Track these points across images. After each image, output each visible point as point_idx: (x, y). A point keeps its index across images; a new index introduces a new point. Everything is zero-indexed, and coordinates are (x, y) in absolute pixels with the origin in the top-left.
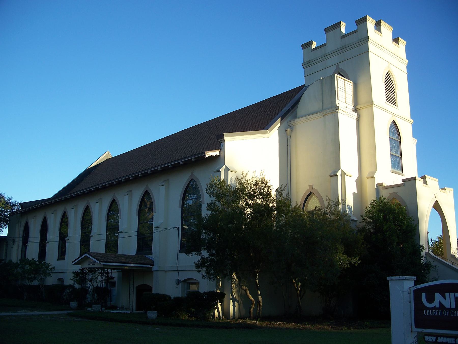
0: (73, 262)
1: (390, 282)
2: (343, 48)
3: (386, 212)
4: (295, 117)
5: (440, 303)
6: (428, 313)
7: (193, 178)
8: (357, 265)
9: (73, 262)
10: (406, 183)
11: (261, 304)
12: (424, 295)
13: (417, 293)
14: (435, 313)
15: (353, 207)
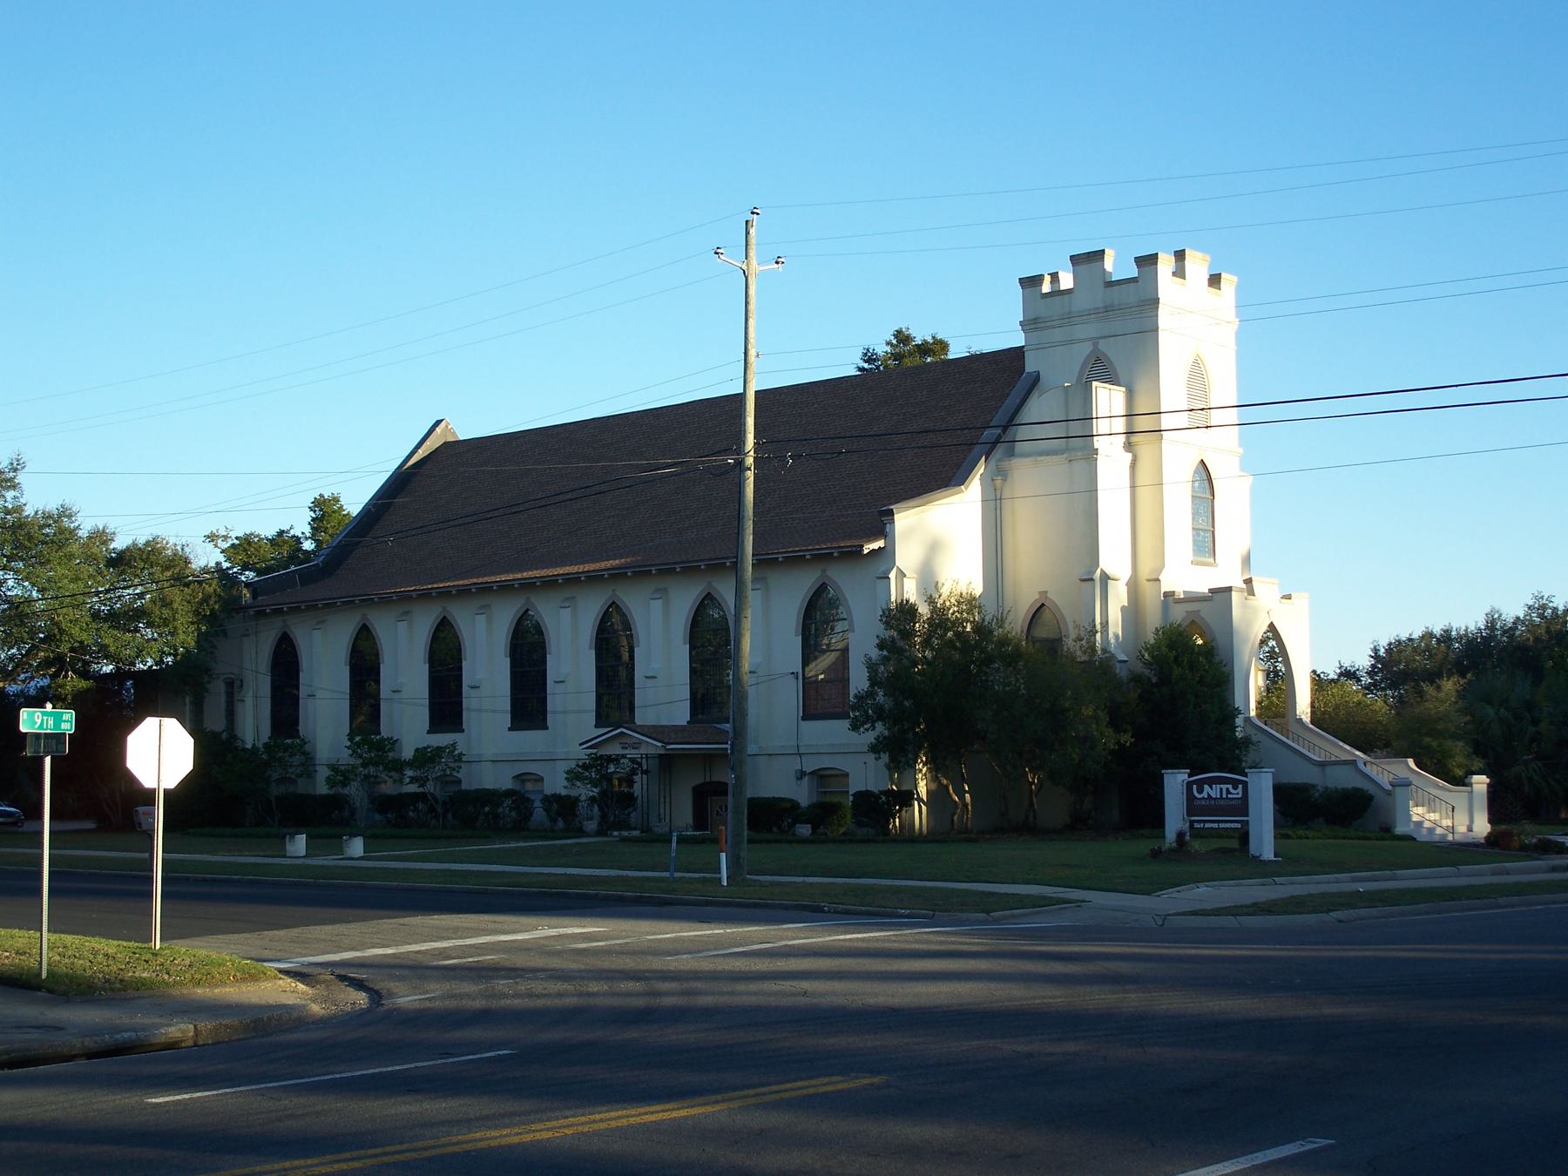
0: (581, 745)
1: (1165, 775)
2: (1108, 310)
3: (1180, 650)
4: (1011, 454)
5: (1209, 794)
6: (1198, 802)
7: (826, 582)
8: (1128, 745)
9: (581, 745)
10: (1215, 595)
11: (970, 808)
12: (1195, 786)
13: (1189, 785)
14: (1203, 803)
15: (1120, 634)
